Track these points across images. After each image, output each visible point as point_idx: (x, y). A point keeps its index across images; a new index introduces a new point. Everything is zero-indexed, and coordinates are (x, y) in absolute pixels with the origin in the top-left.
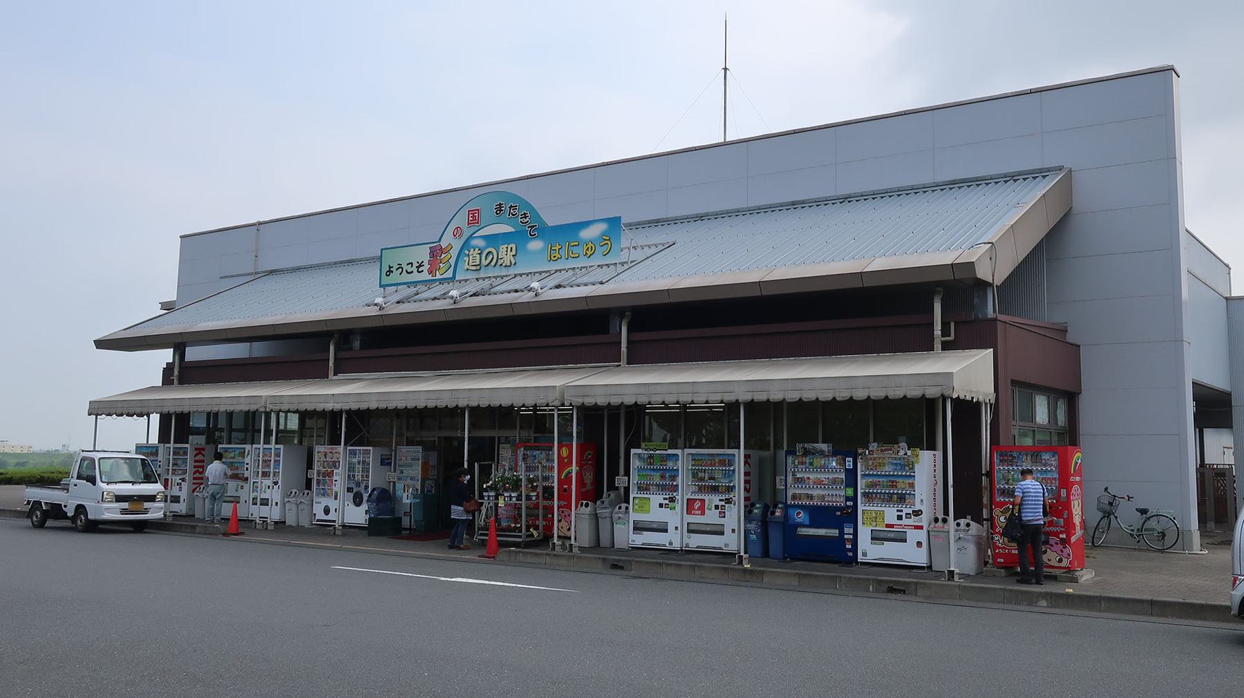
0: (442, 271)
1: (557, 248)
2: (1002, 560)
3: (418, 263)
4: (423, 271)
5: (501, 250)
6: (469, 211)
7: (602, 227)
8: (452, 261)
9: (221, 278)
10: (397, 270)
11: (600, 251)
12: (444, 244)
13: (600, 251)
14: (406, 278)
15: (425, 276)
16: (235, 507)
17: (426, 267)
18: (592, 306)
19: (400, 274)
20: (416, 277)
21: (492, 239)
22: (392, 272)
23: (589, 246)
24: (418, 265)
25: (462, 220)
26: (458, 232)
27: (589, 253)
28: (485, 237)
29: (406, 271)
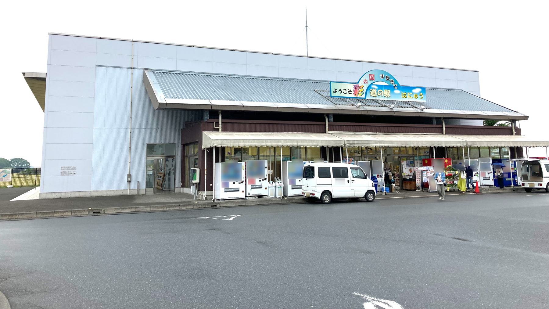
0: (360, 95)
1: (405, 94)
2: (91, 208)
3: (349, 90)
4: (351, 93)
5: (385, 91)
6: (370, 75)
7: (420, 90)
8: (364, 92)
9: (96, 66)
10: (339, 91)
11: (419, 97)
12: (360, 84)
13: (419, 97)
14: (343, 95)
15: (352, 95)
16: (172, 191)
17: (353, 92)
18: (245, 109)
19: (341, 93)
20: (348, 95)
21: (380, 87)
22: (337, 92)
23: (416, 95)
24: (349, 91)
25: (367, 77)
26: (365, 82)
27: (416, 97)
28: (377, 85)
29: (343, 92)
